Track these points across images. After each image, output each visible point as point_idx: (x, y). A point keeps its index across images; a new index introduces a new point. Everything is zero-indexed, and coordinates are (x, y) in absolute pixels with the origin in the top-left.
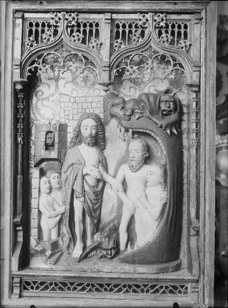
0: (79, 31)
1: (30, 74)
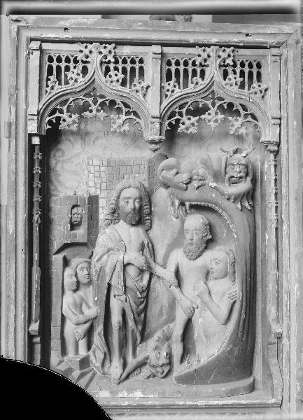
1: (50, 127)
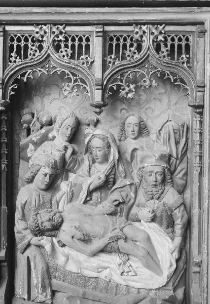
0: (66, 46)
1: (14, 93)
